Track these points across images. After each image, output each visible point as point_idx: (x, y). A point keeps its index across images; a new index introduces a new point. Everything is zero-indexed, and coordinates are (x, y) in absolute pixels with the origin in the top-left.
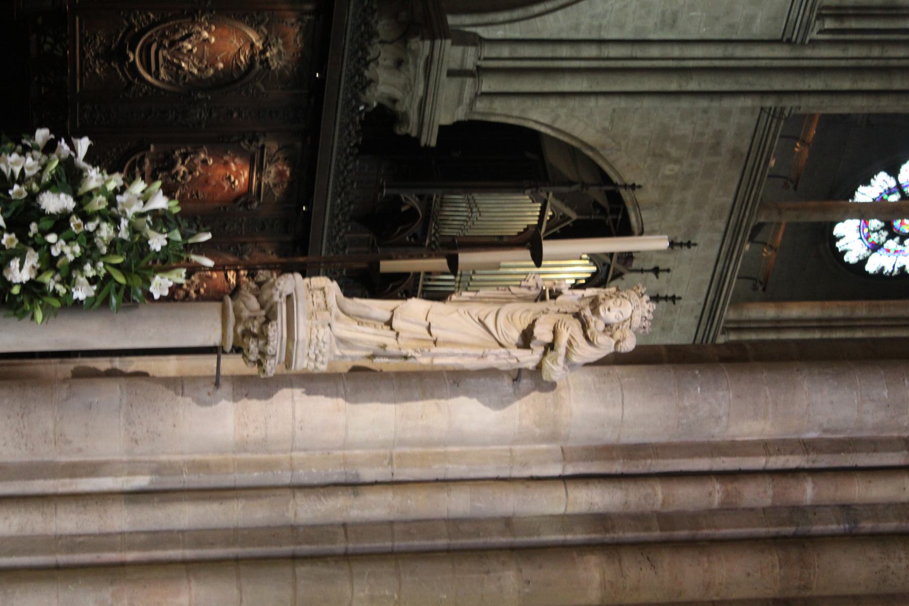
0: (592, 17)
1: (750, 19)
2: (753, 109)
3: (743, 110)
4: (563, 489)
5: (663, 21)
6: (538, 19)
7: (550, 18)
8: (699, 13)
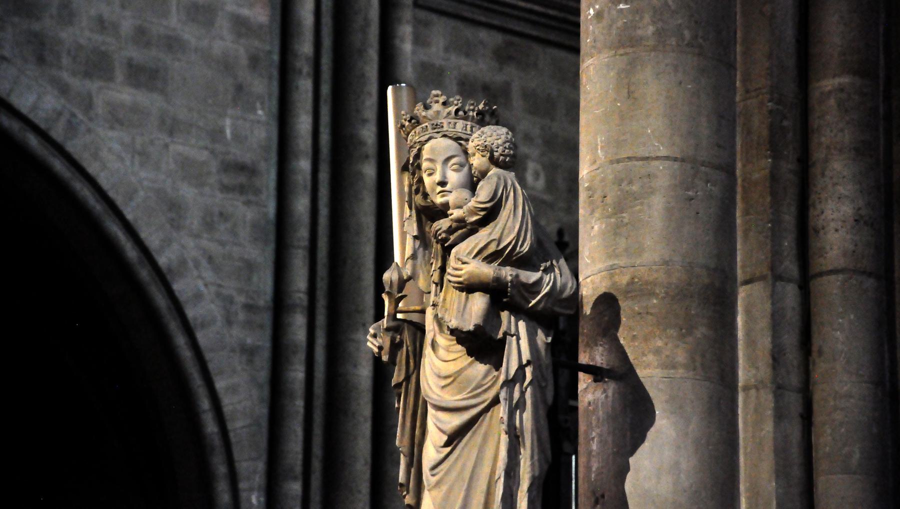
0: (229, 322)
1: (241, 26)
2: (418, 23)
3: (419, 41)
4: (819, 280)
5: (241, 189)
6: (230, 426)
7: (228, 403)
8: (228, 122)
